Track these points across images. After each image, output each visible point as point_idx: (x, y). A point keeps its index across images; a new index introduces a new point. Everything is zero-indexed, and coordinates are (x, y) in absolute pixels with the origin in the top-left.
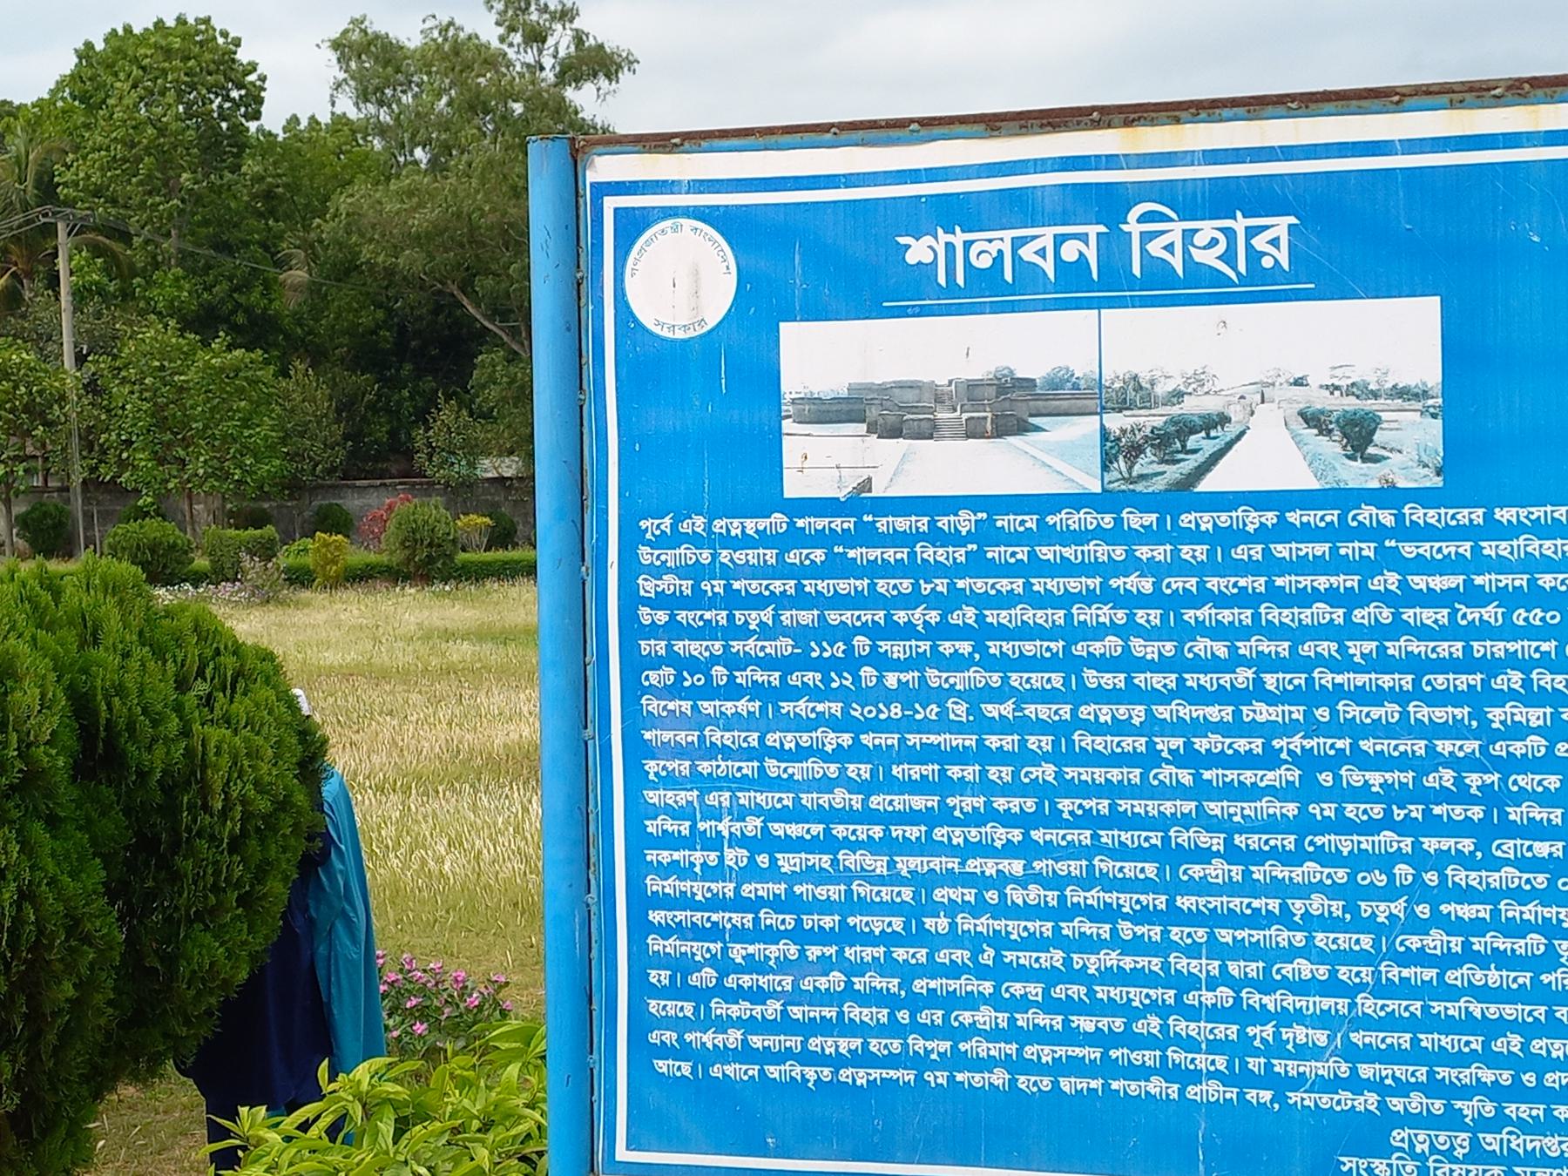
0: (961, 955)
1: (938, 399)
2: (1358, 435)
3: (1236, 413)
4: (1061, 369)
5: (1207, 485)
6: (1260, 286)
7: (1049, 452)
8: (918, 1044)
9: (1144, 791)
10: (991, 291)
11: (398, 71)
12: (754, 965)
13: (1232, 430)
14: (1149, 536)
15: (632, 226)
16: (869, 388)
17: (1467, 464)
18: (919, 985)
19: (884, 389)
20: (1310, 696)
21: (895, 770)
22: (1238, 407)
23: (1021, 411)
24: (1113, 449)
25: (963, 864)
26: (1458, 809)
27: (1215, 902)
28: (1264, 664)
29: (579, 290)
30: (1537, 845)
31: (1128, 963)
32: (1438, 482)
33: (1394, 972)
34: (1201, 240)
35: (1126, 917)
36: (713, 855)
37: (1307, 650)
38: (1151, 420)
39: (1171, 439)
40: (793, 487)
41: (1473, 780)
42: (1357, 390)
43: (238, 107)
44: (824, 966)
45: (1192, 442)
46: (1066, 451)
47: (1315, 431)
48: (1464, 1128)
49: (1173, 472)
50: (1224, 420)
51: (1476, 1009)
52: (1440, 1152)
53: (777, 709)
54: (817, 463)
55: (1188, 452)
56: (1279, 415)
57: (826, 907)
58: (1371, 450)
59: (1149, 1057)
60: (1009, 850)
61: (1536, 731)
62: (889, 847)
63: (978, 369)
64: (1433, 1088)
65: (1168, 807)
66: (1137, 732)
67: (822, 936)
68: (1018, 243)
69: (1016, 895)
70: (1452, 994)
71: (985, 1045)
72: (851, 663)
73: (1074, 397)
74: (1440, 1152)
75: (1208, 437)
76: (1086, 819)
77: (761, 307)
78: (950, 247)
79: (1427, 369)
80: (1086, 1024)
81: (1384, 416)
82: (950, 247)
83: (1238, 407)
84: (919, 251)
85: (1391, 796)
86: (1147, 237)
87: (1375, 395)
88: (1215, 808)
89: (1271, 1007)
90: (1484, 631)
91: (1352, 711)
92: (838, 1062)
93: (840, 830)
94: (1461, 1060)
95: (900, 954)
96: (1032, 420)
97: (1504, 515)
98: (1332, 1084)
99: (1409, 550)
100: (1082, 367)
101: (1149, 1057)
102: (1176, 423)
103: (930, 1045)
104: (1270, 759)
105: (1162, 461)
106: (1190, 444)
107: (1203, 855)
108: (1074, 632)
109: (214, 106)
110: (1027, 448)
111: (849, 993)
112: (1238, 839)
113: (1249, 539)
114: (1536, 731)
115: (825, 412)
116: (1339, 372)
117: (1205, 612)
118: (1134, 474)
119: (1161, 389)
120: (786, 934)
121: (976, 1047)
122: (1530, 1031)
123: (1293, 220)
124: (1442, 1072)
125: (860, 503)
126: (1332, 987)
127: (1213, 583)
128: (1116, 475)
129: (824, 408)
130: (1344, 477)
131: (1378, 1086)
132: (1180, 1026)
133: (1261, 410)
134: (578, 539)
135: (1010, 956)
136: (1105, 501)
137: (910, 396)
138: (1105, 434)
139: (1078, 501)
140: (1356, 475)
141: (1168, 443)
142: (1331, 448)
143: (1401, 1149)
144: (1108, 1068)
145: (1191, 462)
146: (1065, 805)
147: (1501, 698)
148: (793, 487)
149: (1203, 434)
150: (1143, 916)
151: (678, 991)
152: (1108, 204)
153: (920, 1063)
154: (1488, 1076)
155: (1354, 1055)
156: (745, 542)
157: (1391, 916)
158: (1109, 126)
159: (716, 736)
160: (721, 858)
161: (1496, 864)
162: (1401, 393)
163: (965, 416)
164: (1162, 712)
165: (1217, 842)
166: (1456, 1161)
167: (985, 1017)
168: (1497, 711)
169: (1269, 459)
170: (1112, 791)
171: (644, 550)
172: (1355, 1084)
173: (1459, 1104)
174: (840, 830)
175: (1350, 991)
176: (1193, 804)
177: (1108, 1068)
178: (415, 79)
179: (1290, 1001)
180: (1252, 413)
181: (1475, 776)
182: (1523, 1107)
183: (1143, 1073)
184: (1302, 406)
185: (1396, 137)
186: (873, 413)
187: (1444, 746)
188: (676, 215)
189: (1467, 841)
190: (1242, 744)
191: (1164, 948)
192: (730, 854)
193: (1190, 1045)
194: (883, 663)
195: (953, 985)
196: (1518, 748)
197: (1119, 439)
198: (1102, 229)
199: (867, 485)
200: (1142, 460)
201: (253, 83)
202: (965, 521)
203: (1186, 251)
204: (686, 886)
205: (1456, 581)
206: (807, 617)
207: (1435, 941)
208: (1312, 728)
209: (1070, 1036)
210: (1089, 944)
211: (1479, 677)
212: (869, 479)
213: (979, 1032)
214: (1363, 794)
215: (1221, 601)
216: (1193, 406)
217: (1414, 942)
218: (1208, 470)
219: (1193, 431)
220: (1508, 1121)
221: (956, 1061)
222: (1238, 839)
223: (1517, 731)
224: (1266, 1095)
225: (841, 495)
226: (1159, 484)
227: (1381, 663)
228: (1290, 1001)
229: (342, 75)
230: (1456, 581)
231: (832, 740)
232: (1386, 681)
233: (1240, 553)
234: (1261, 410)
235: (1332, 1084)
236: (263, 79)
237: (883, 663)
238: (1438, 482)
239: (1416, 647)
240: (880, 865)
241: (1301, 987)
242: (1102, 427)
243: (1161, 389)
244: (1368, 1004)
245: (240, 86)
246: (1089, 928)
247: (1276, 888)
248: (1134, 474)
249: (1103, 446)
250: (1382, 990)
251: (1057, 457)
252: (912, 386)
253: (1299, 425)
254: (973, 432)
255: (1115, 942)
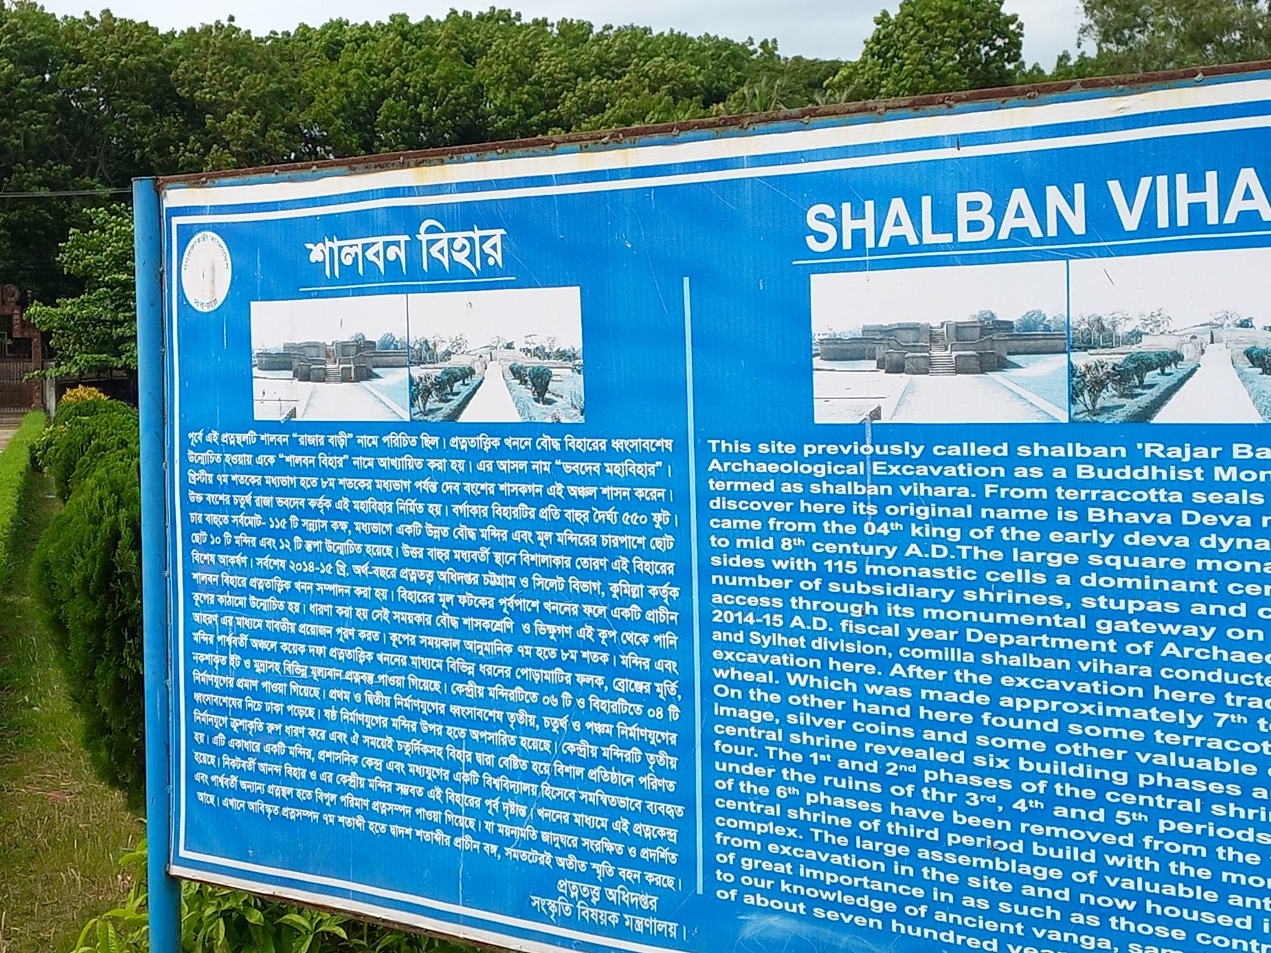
0: (342, 736)
1: (933, 337)
2: (539, 383)
3: (1188, 352)
4: (1034, 313)
5: (1160, 418)
6: (487, 279)
7: (382, 392)
8: (321, 795)
9: (434, 631)
10: (354, 281)
11: (1137, 15)
12: (243, 734)
13: (1184, 367)
14: (435, 453)
15: (187, 233)
16: (293, 347)
17: (600, 407)
18: (322, 754)
19: (301, 347)
20: (518, 569)
21: (312, 607)
22: (1190, 347)
23: (1000, 349)
24: (1078, 385)
25: (344, 674)
26: (596, 654)
27: (470, 710)
28: (495, 545)
29: (159, 280)
30: (637, 683)
31: (426, 749)
32: (581, 419)
33: (561, 768)
34: (457, 245)
35: (424, 717)
36: (224, 658)
37: (516, 536)
38: (1113, 358)
39: (1129, 375)
40: (261, 412)
41: (603, 634)
42: (540, 352)
43: (1003, 53)
44: (276, 737)
45: (1149, 377)
46: (389, 391)
47: (1260, 370)
48: (597, 883)
49: (1132, 405)
50: (1177, 357)
51: (604, 798)
52: (584, 899)
53: (255, 562)
54: (273, 395)
55: (1145, 387)
56: (1226, 355)
57: (276, 697)
58: (547, 396)
59: (434, 815)
60: (366, 667)
61: (636, 601)
62: (307, 659)
63: (964, 313)
64: (581, 853)
65: (446, 642)
66: (428, 589)
67: (274, 717)
68: (366, 247)
69: (371, 698)
70: (591, 786)
71: (353, 799)
72: (288, 533)
73: (1045, 337)
74: (584, 899)
75: (464, 384)
76: (404, 648)
77: (245, 290)
78: (331, 250)
79: (572, 339)
80: (404, 789)
81: (554, 371)
82: (331, 250)
83: (1190, 347)
84: (317, 253)
85: (563, 643)
86: (431, 243)
87: (548, 356)
88: (469, 645)
89: (497, 787)
90: (606, 528)
91: (539, 580)
92: (281, 802)
93: (285, 646)
94: (596, 834)
95: (313, 732)
96: (375, 370)
97: (617, 444)
98: (527, 844)
99: (568, 467)
100: (1052, 311)
101: (434, 815)
102: (1134, 361)
103: (327, 795)
104: (497, 613)
105: (1122, 396)
106: (455, 389)
107: (463, 678)
108: (399, 518)
109: (983, 52)
110: (1010, 385)
111: (287, 758)
112: (482, 667)
113: (487, 456)
114: (636, 601)
115: (846, 351)
116: (529, 340)
117: (463, 507)
118: (1098, 406)
119: (440, 350)
120: (256, 714)
121: (349, 800)
122: (634, 817)
123: (503, 232)
124: (586, 842)
125: (290, 425)
126: (529, 776)
127: (468, 487)
128: (1082, 407)
129: (844, 347)
130: (533, 414)
131: (550, 848)
132: (453, 796)
133: (1210, 348)
134: (160, 444)
135: (366, 739)
136: (412, 427)
137: (314, 352)
138: (1072, 370)
139: (397, 427)
140: (541, 414)
141: (1124, 379)
142: (527, 393)
143: (563, 894)
144: (414, 821)
145: (1148, 396)
146: (394, 637)
147: (617, 576)
148: (261, 412)
149: (1159, 371)
150: (433, 717)
151: (208, 748)
152: (407, 220)
153: (320, 807)
154: (610, 847)
155: (540, 824)
156: (235, 450)
157: (560, 728)
158: (408, 167)
159: (228, 579)
160: (228, 660)
161: (614, 696)
162: (562, 355)
163: (954, 354)
164: (443, 575)
165: (469, 669)
166: (591, 905)
167: (353, 779)
168: (615, 585)
169: (495, 402)
170: (418, 629)
171: (190, 452)
172: (540, 845)
173: (594, 866)
174: (285, 646)
175: (538, 779)
176: (459, 641)
177: (414, 821)
178: (1151, 20)
179: (509, 784)
180: (1203, 352)
181: (604, 631)
182: (629, 871)
183: (430, 826)
184: (1248, 346)
185: (553, 173)
186: (880, 351)
187: (588, 609)
188: (204, 230)
189: (600, 678)
190: (483, 601)
191: (443, 740)
192: (232, 657)
193: (456, 809)
194: (305, 535)
195: (339, 756)
196: (626, 612)
197: (1085, 375)
198: (407, 238)
199: (293, 413)
200: (1104, 394)
201: (1013, 32)
202: (341, 439)
203: (450, 253)
204: (211, 677)
205: (591, 491)
206: (267, 501)
207: (583, 748)
208: (520, 592)
209: (395, 797)
210: (405, 735)
211: (605, 560)
212: (879, 408)
213: (350, 790)
214: (544, 640)
215: (473, 500)
216: (1149, 345)
217: (572, 747)
218: (464, 407)
219: (1150, 368)
220: (621, 881)
221: (339, 809)
222: (482, 667)
223: (625, 601)
224: (494, 848)
225: (281, 418)
226: (1119, 416)
227: (554, 548)
228: (509, 784)
229: (1088, 21)
230: (591, 491)
231: (283, 585)
232: (557, 560)
233: (481, 466)
234: (1210, 348)
235: (527, 844)
236: (1021, 26)
237: (305, 535)
238: (581, 419)
239: (572, 537)
240: (302, 671)
241: (513, 774)
242: (1070, 364)
243: (440, 350)
244: (547, 790)
245: (1003, 35)
246: (405, 723)
247: (502, 704)
248: (1098, 406)
249: (1070, 381)
250: (556, 780)
251: (382, 399)
252: (915, 328)
253: (1245, 364)
254: (961, 368)
255: (419, 734)
